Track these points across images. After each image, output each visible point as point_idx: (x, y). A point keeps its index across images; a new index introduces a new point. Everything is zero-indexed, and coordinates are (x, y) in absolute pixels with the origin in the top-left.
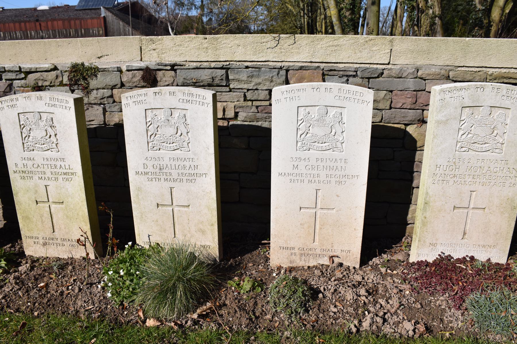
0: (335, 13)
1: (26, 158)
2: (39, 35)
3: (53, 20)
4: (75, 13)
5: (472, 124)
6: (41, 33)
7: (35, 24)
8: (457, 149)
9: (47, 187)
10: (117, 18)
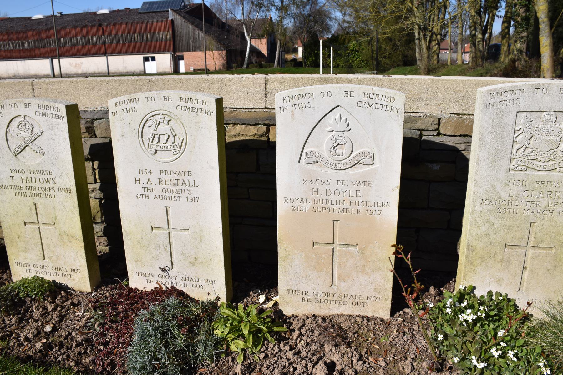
0: (545, 8)
1: (139, 195)
2: (101, 41)
3: (117, 24)
4: (139, 16)
5: (531, 135)
6: (103, 38)
7: (98, 29)
8: (512, 167)
9: (37, 204)
10: (187, 21)
